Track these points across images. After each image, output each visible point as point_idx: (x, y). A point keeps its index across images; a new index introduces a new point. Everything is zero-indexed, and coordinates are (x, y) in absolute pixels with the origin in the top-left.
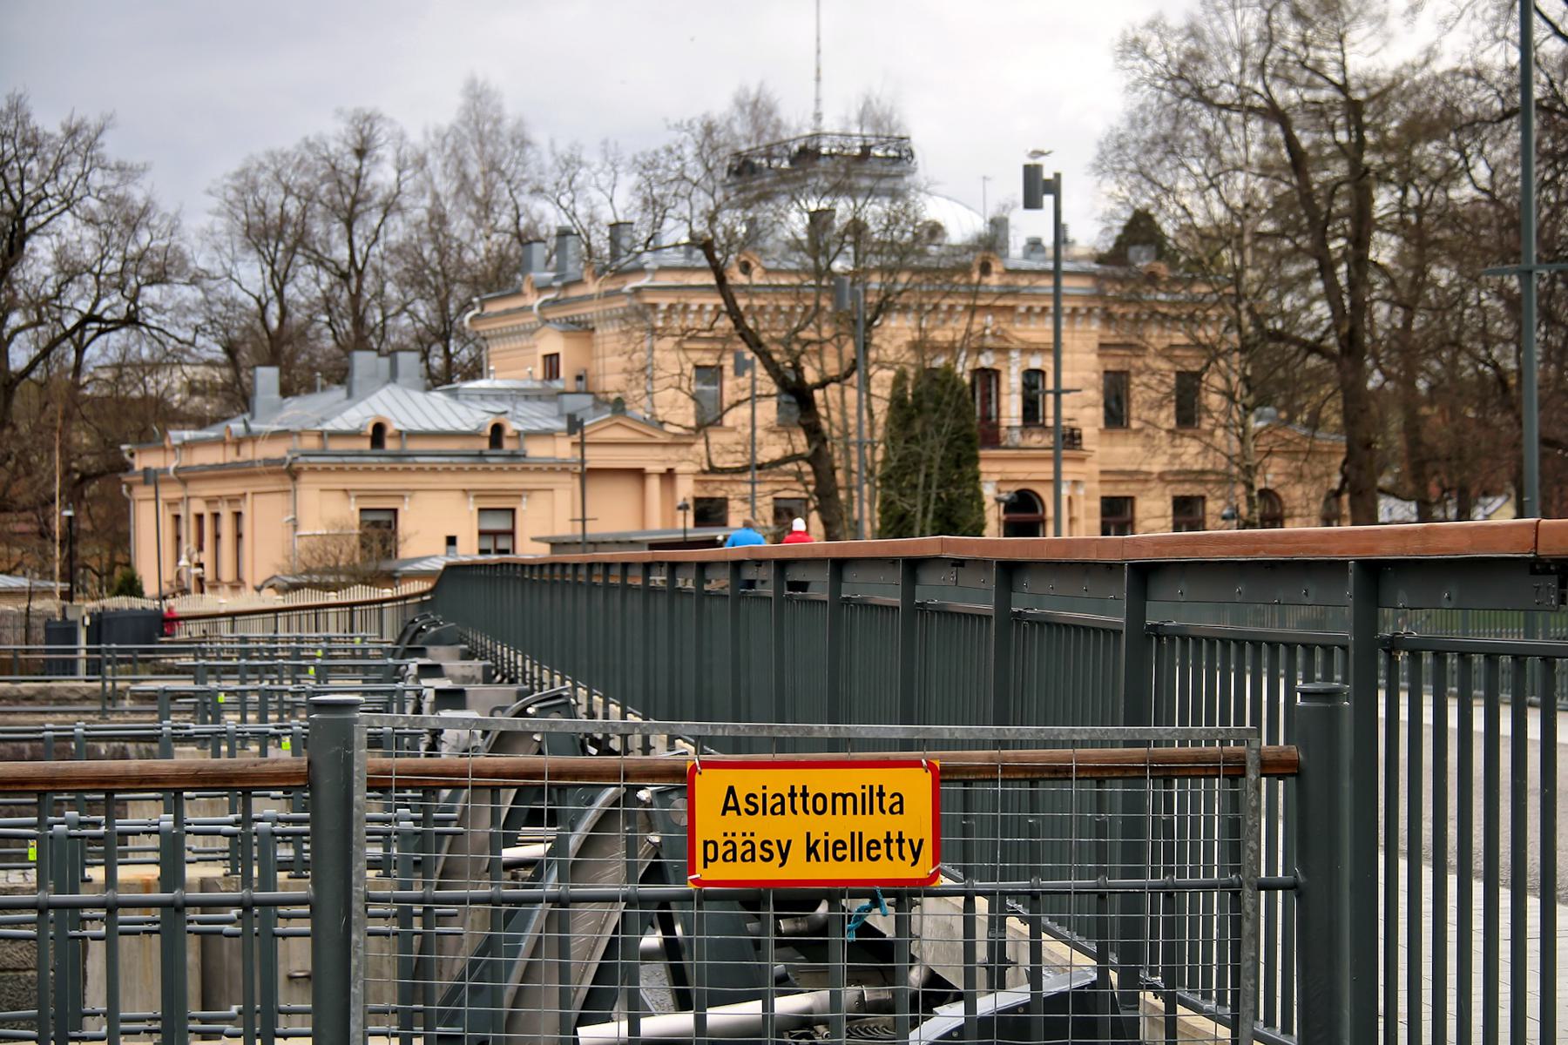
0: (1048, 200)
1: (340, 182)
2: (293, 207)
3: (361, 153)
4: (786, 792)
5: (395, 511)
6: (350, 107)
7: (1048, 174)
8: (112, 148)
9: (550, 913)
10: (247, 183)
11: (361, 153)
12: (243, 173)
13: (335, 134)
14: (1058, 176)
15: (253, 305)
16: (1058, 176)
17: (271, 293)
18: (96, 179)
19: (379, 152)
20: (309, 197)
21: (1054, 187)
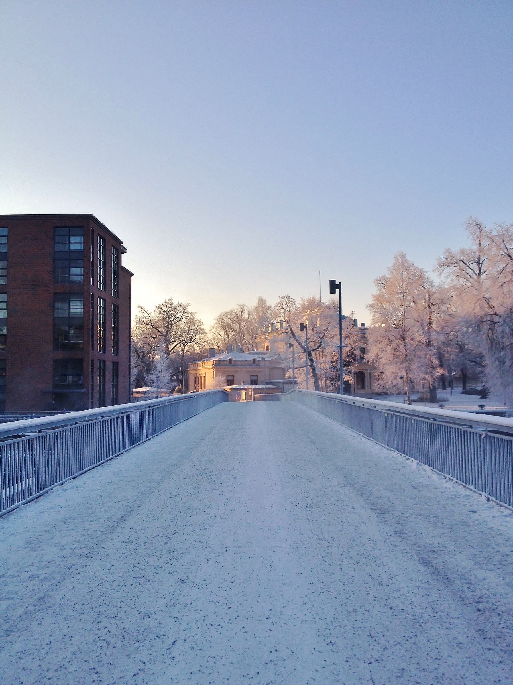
0: (337, 291)
1: (238, 317)
2: (230, 321)
3: (242, 312)
4: (107, 618)
5: (257, 376)
6: (239, 304)
7: (337, 283)
8: (189, 309)
9: (357, 389)
10: (183, 308)
11: (242, 312)
12: (220, 316)
13: (236, 309)
14: (340, 283)
15: (223, 339)
16: (340, 283)
17: (226, 336)
18: (186, 315)
19: (245, 311)
20: (232, 320)
21: (339, 287)
